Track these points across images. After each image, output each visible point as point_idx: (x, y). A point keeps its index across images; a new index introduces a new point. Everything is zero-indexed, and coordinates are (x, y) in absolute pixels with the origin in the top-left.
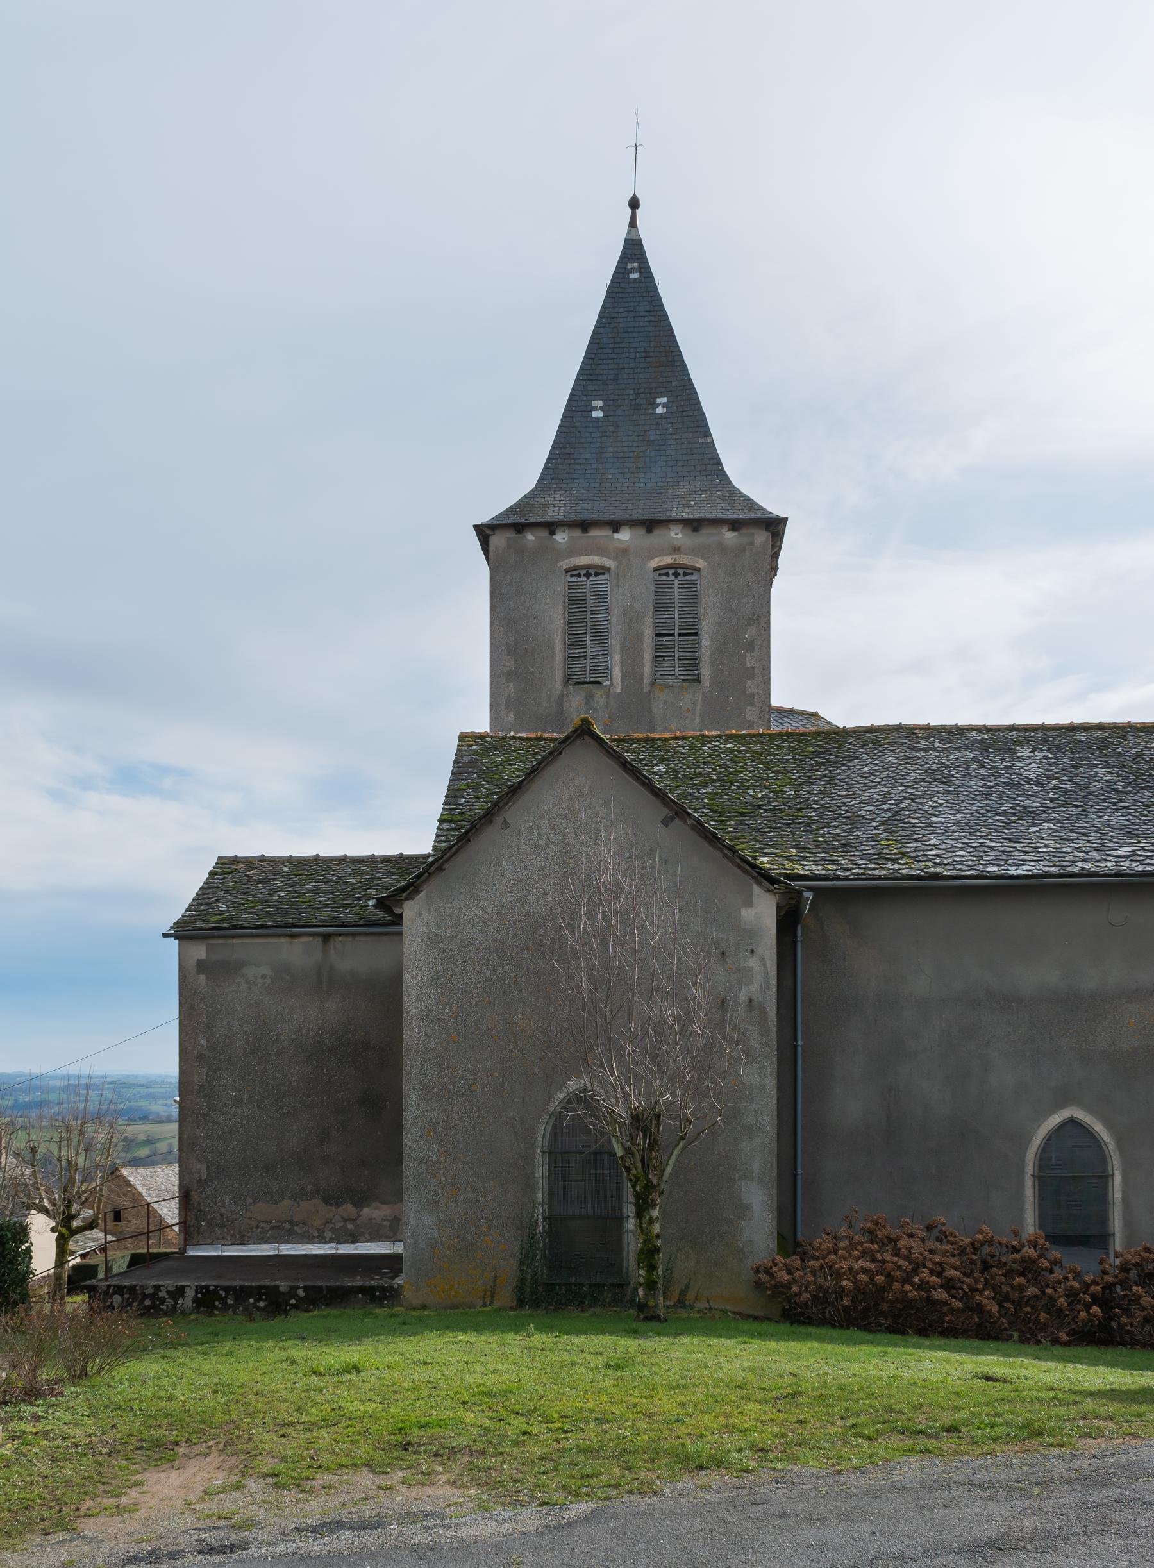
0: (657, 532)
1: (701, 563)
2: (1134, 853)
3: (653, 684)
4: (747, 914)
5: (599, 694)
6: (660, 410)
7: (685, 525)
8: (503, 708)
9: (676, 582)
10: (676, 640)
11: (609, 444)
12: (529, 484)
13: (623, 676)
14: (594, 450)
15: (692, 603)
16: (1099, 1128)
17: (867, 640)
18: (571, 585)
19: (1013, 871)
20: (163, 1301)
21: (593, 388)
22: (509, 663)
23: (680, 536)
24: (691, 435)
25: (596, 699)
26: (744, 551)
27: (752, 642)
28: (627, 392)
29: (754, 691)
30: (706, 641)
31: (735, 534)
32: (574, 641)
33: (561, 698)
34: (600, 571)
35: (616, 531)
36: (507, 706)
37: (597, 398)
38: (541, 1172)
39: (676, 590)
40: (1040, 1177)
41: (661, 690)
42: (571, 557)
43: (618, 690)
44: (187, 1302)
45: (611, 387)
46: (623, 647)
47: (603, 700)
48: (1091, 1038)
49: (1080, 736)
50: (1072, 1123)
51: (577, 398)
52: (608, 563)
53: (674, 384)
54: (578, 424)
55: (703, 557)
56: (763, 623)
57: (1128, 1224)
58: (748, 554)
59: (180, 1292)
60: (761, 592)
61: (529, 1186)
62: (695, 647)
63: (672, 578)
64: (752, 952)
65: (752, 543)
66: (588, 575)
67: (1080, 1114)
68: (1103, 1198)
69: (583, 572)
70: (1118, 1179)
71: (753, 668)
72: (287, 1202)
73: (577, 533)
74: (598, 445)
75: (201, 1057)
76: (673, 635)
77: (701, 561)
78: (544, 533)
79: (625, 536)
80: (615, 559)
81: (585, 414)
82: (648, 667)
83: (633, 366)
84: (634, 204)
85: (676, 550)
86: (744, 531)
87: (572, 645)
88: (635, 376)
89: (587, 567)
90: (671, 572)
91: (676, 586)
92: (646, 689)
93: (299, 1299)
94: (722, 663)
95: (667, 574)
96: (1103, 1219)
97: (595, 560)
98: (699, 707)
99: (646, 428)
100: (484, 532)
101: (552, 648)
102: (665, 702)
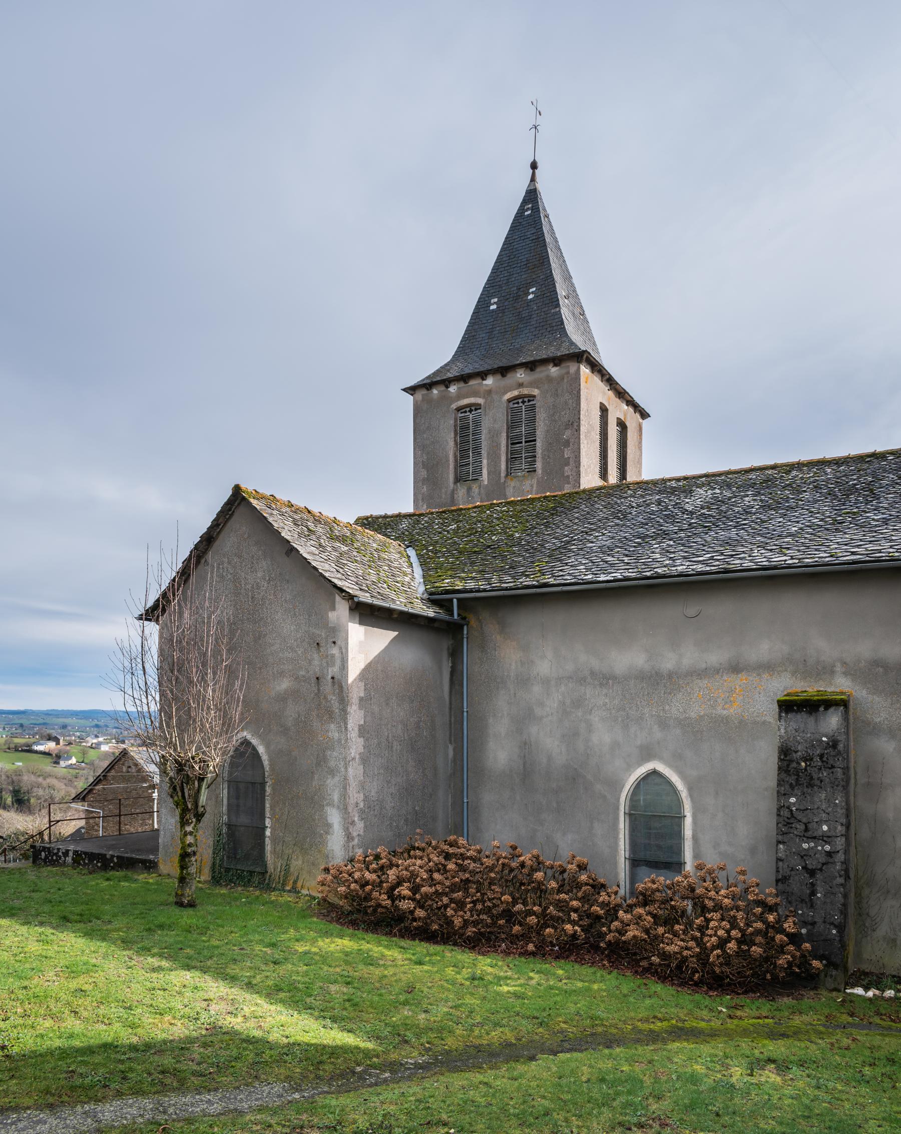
0: (509, 375)
1: (536, 392)
2: (712, 558)
3: (507, 475)
4: (332, 615)
5: (475, 488)
6: (531, 296)
7: (527, 367)
10: (521, 448)
13: (489, 474)
15: (532, 421)
22: (424, 473)
30: (539, 444)
33: (453, 490)
34: (477, 407)
36: (423, 499)
40: (630, 815)
43: (486, 483)
46: (488, 454)
47: (477, 490)
48: (667, 707)
49: (752, 476)
52: (480, 401)
55: (537, 388)
57: (696, 856)
59: (66, 854)
63: (521, 404)
64: (334, 643)
65: (568, 373)
66: (471, 411)
67: (661, 768)
68: (678, 835)
69: (468, 409)
73: (462, 384)
78: (442, 388)
79: (489, 381)
80: (484, 397)
84: (534, 166)
85: (521, 385)
86: (563, 365)
89: (469, 405)
90: (520, 401)
92: (502, 480)
93: (115, 864)
94: (549, 457)
95: (518, 403)
97: (472, 400)
100: (412, 390)
101: (448, 461)
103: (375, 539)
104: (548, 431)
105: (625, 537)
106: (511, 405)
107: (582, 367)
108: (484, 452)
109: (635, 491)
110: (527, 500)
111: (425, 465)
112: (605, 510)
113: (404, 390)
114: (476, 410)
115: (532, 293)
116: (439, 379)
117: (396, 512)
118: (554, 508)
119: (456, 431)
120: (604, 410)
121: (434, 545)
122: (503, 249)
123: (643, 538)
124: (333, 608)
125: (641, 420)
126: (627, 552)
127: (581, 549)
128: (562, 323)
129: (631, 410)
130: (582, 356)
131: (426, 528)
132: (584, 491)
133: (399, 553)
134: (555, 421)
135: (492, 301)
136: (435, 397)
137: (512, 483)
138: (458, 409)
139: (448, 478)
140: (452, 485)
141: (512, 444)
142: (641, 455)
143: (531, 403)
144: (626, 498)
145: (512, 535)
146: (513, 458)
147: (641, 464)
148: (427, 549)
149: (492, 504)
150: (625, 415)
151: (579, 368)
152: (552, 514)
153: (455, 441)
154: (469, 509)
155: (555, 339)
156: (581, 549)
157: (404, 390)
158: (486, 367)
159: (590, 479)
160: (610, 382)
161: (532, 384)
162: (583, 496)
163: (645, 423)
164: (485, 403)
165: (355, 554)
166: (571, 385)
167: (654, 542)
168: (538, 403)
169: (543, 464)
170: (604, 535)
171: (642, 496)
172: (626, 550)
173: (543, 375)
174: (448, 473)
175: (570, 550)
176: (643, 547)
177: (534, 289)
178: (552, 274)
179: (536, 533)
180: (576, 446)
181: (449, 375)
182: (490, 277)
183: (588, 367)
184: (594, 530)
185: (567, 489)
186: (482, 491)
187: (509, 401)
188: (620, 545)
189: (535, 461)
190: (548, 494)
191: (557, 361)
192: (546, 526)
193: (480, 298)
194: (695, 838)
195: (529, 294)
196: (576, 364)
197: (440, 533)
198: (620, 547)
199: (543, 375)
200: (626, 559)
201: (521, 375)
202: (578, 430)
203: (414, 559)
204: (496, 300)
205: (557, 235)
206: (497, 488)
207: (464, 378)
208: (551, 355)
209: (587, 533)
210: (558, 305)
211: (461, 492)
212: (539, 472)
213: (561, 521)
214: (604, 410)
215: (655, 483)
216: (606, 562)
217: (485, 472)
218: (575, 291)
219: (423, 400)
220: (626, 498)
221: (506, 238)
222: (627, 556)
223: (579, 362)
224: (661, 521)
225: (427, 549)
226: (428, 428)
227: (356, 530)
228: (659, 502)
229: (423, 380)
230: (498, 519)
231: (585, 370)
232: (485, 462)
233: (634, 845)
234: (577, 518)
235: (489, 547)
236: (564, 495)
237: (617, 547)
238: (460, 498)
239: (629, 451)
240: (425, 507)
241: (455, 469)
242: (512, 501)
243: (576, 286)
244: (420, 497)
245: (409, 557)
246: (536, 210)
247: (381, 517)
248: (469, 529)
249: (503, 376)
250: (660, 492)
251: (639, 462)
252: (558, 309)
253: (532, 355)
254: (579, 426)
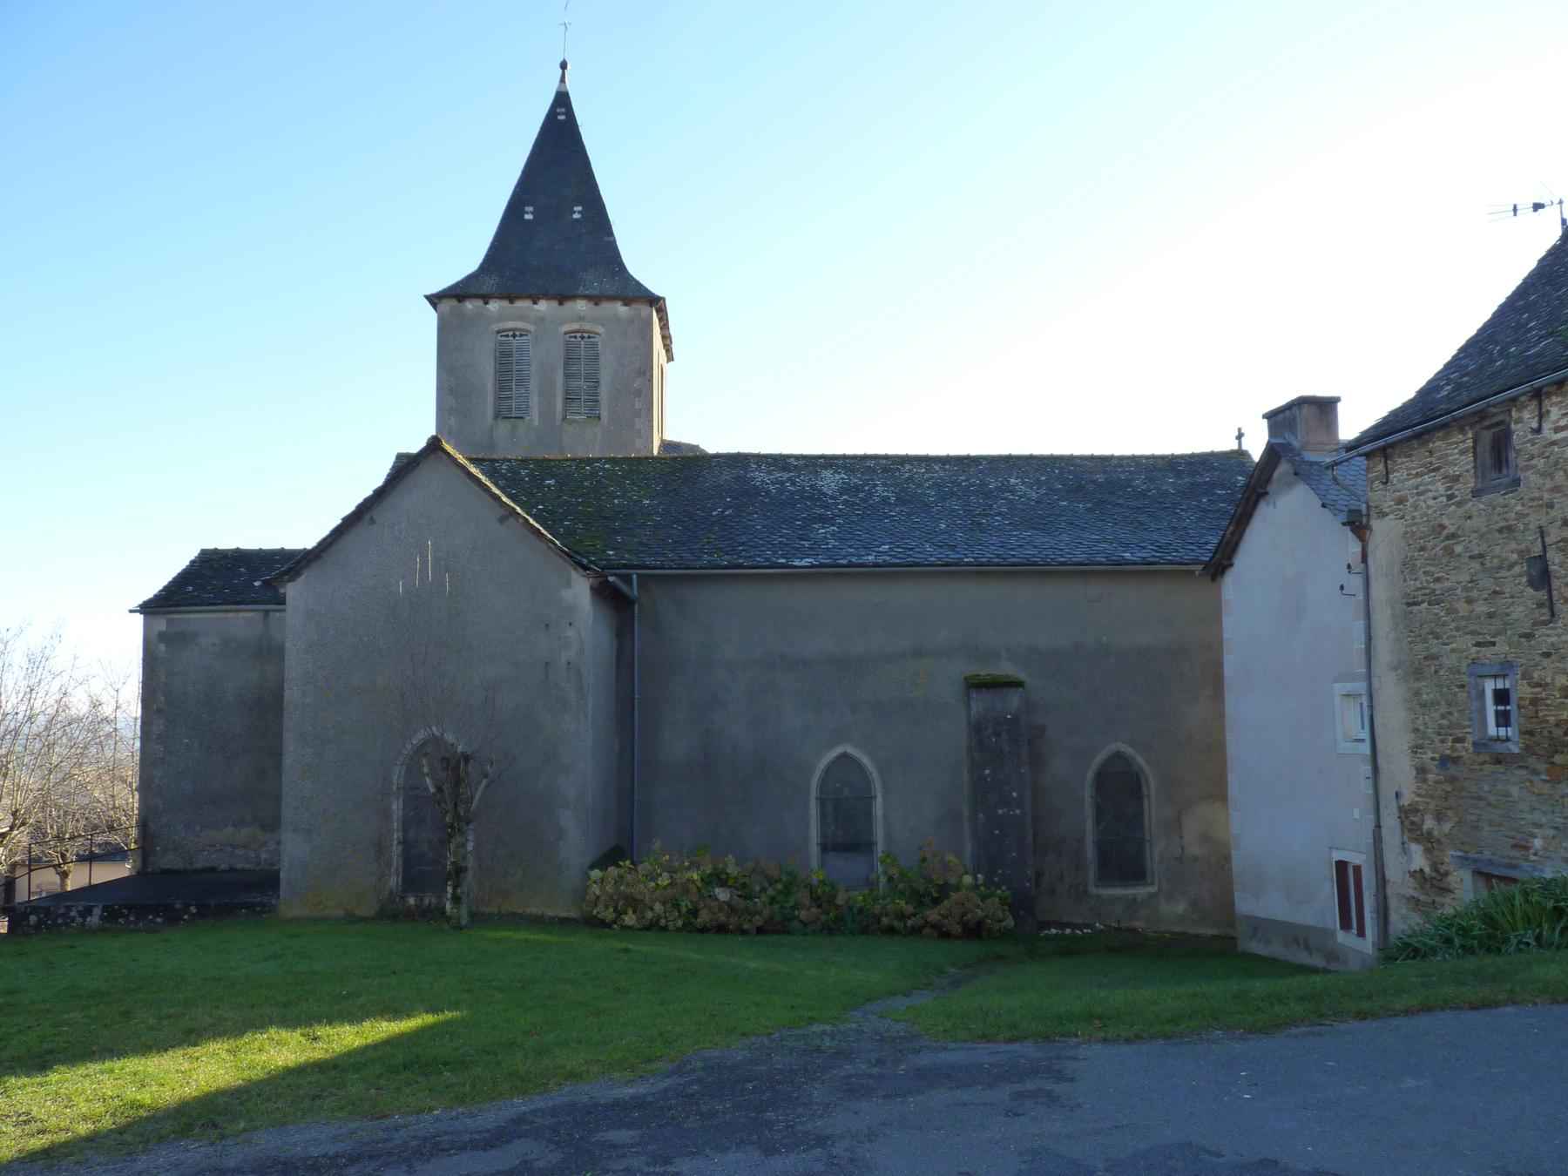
1: (600, 330)
3: (564, 419)
4: (567, 594)
13: (540, 415)
15: (595, 358)
16: (865, 760)
17: (734, 386)
19: (797, 563)
20: (73, 919)
32: (502, 384)
38: (397, 807)
43: (536, 423)
44: (94, 920)
50: (845, 756)
57: (888, 836)
61: (386, 815)
66: (514, 336)
67: (851, 750)
68: (869, 814)
70: (879, 799)
72: (230, 830)
75: (159, 711)
78: (479, 303)
84: (564, 66)
87: (501, 389)
92: (558, 422)
96: (870, 832)
97: (519, 325)
100: (434, 300)
124: (568, 584)
161: (596, 321)
194: (885, 817)
211: (504, 427)
212: (604, 418)
232: (535, 399)
233: (823, 835)
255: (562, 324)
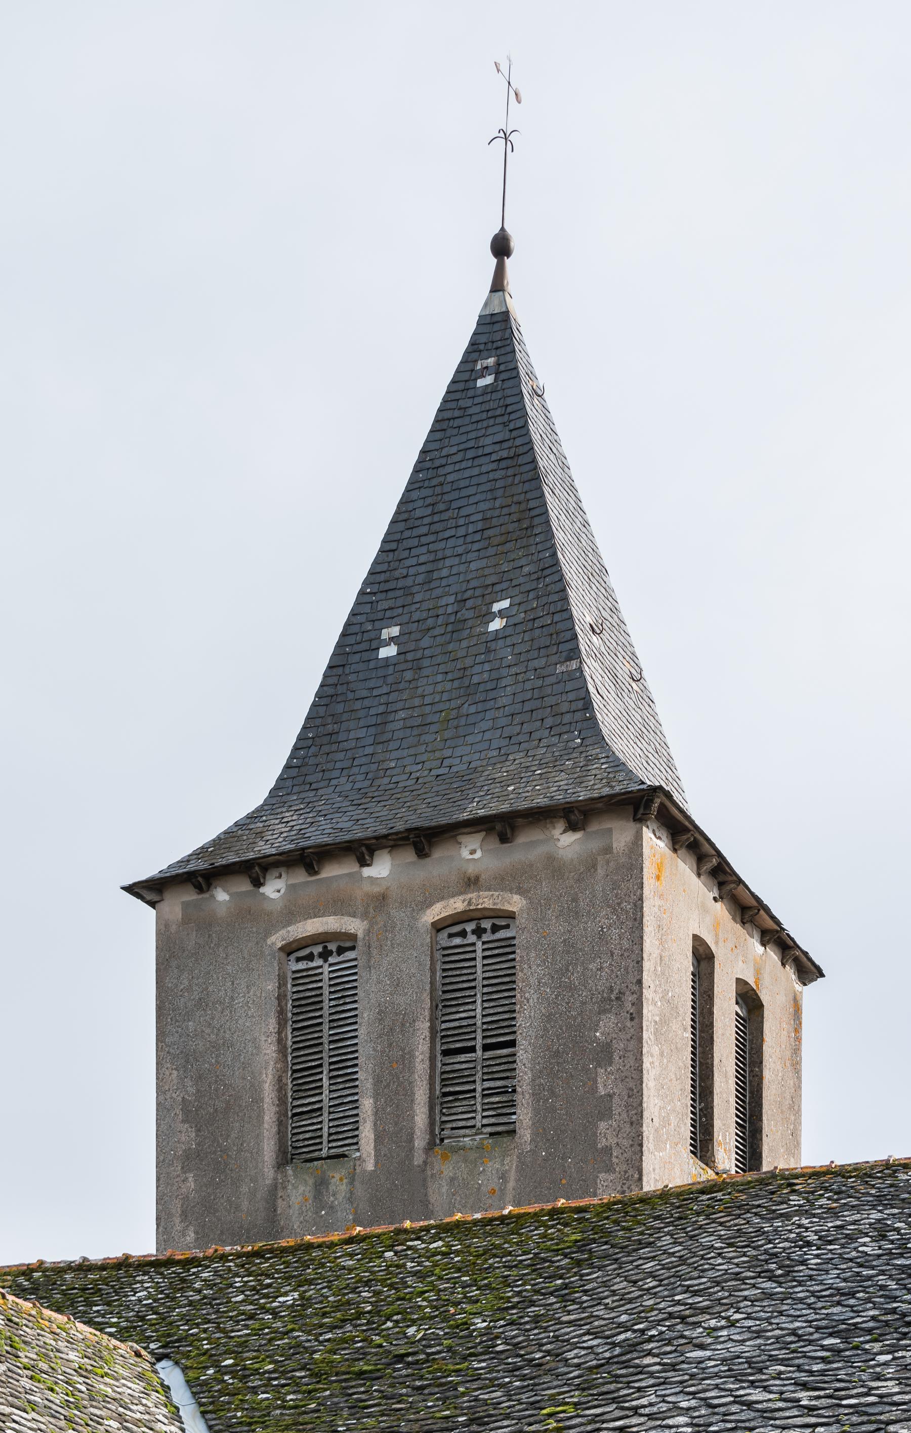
0: (438, 853)
1: (515, 903)
3: (431, 1146)
5: (337, 1177)
6: (496, 625)
7: (489, 831)
8: (177, 1220)
9: (479, 945)
10: (472, 1062)
11: (400, 705)
12: (257, 797)
13: (379, 1139)
14: (373, 721)
15: (504, 986)
18: (298, 977)
21: (385, 605)
22: (187, 1136)
23: (478, 855)
24: (542, 662)
25: (332, 1188)
26: (594, 866)
27: (609, 1045)
28: (443, 602)
29: (613, 1141)
30: (524, 1054)
31: (578, 835)
32: (301, 1076)
34: (345, 943)
35: (364, 863)
36: (184, 1215)
37: (390, 621)
39: (479, 963)
41: (445, 1157)
42: (289, 923)
43: (370, 1166)
45: (418, 598)
46: (378, 1081)
47: (343, 1188)
51: (355, 629)
52: (354, 925)
53: (526, 570)
54: (352, 678)
55: (520, 891)
56: (628, 1006)
58: (601, 872)
60: (626, 944)
62: (509, 1068)
63: (472, 938)
65: (608, 850)
71: (610, 1096)
73: (300, 876)
74: (382, 709)
76: (472, 1049)
77: (516, 897)
78: (243, 885)
79: (381, 869)
80: (365, 916)
81: (366, 656)
82: (421, 1119)
83: (460, 550)
84: (501, 247)
85: (472, 883)
86: (594, 826)
87: (298, 1090)
88: (462, 568)
90: (470, 927)
91: (479, 954)
92: (418, 1158)
94: (553, 1093)
95: (463, 934)
98: (511, 1184)
99: (468, 662)
100: (149, 890)
101: (258, 1100)
102: (452, 1179)
103: (70, 1338)
104: (549, 1018)
105: (794, 1333)
106: (443, 939)
107: (648, 834)
108: (365, 1078)
109: (810, 1196)
110: (503, 1219)
111: (191, 1114)
112: (730, 1252)
113: (131, 889)
114: (341, 951)
115: (501, 613)
116: (232, 858)
117: (116, 1253)
118: (580, 1246)
119: (281, 1012)
120: (703, 958)
121: (236, 1355)
122: (413, 485)
123: (844, 1335)
125: (798, 987)
126: (803, 1377)
127: (673, 1367)
128: (587, 704)
129: (773, 956)
130: (650, 801)
131: (208, 1301)
132: (664, 1195)
133: (140, 1377)
134: (571, 988)
135: (385, 634)
136: (222, 912)
137: (447, 1168)
138: (289, 950)
139: (260, 1152)
140: (269, 1172)
141: (446, 1053)
142: (798, 1087)
143: (501, 934)
144: (787, 1216)
145: (466, 1324)
146: (448, 1094)
147: (798, 1113)
148: (216, 1365)
149: (399, 1232)
150: (758, 973)
151: (639, 837)
152: (579, 1263)
153: (280, 1041)
154: (331, 1245)
155: (568, 751)
156: (673, 1367)
157: (131, 889)
158: (372, 828)
159: (668, 1164)
160: (720, 874)
161: (507, 881)
162: (663, 1210)
163: (810, 993)
164: (368, 932)
165: (26, 1383)
166: (615, 886)
167: (877, 1347)
168: (522, 934)
169: (536, 1111)
170: (732, 1324)
171: (833, 1213)
172: (799, 1368)
173: (534, 855)
174: (259, 1137)
175: (641, 1370)
176: (848, 1361)
177: (505, 604)
178: (557, 563)
179: (536, 1319)
180: (631, 1061)
181: (264, 848)
182: (376, 562)
183: (664, 834)
184: (704, 1310)
185: (607, 1191)
186: (360, 1191)
187: (438, 927)
188: (782, 1354)
189: (512, 1104)
190: (561, 1202)
191: (576, 815)
192: (563, 1299)
193: (348, 625)
195: (491, 616)
196: (631, 826)
197: (252, 1317)
198: (782, 1362)
199: (534, 855)
200: (805, 1397)
201: (472, 852)
202: (636, 1016)
203: (181, 1395)
204: (395, 631)
205: (566, 449)
206: (403, 1181)
207: (308, 859)
208: (559, 797)
209: (683, 1319)
210: (574, 653)
211: (298, 1192)
212: (525, 1134)
213: (605, 1284)
214: (703, 958)
215: (864, 1173)
216: (749, 1405)
217: (367, 1134)
218: (614, 610)
219: (186, 920)
220: (787, 1216)
221: (423, 452)
222: (805, 1386)
223: (640, 819)
224: (893, 1285)
225: (216, 1365)
226: (201, 1004)
227: (19, 1312)
228: (881, 1232)
229: (186, 861)
230: (420, 1275)
231: (654, 843)
232: (367, 1104)
234: (652, 1275)
235: (400, 1358)
236: (609, 1206)
237: (773, 1359)
238: (294, 1212)
239: (767, 1075)
240: (191, 1236)
241: (280, 1124)
242: (458, 1224)
243: (619, 595)
244: (176, 1207)
245: (166, 1389)
246: (509, 372)
247: (70, 1267)
248: (337, 1306)
249: (422, 853)
250: (880, 1201)
251: (794, 1107)
252: (574, 665)
253: (500, 798)
254: (639, 1004)
255: (427, 904)
